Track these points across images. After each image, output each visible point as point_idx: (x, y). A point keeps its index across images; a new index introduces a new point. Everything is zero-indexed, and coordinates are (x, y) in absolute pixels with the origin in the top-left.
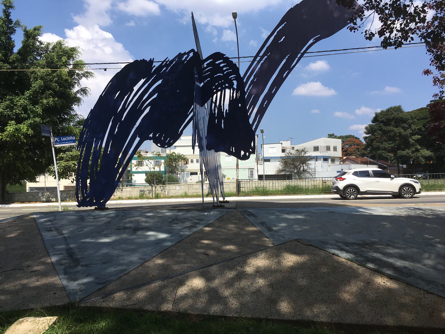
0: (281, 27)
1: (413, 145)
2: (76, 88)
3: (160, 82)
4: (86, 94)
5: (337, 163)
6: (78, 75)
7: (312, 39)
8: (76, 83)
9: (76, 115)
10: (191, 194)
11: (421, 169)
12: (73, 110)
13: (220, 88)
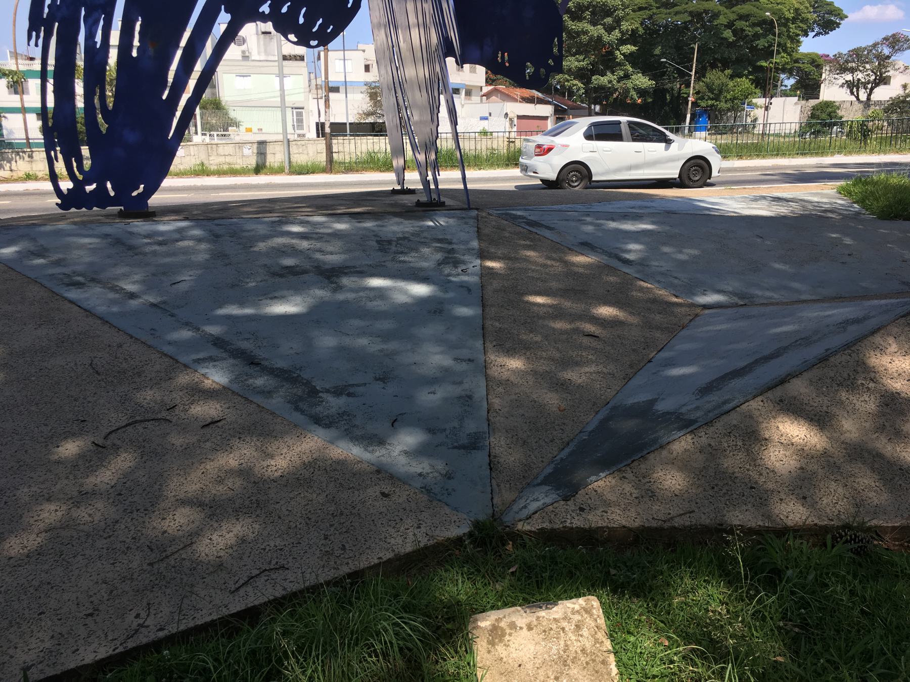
5: (475, 98)
10: (216, 168)
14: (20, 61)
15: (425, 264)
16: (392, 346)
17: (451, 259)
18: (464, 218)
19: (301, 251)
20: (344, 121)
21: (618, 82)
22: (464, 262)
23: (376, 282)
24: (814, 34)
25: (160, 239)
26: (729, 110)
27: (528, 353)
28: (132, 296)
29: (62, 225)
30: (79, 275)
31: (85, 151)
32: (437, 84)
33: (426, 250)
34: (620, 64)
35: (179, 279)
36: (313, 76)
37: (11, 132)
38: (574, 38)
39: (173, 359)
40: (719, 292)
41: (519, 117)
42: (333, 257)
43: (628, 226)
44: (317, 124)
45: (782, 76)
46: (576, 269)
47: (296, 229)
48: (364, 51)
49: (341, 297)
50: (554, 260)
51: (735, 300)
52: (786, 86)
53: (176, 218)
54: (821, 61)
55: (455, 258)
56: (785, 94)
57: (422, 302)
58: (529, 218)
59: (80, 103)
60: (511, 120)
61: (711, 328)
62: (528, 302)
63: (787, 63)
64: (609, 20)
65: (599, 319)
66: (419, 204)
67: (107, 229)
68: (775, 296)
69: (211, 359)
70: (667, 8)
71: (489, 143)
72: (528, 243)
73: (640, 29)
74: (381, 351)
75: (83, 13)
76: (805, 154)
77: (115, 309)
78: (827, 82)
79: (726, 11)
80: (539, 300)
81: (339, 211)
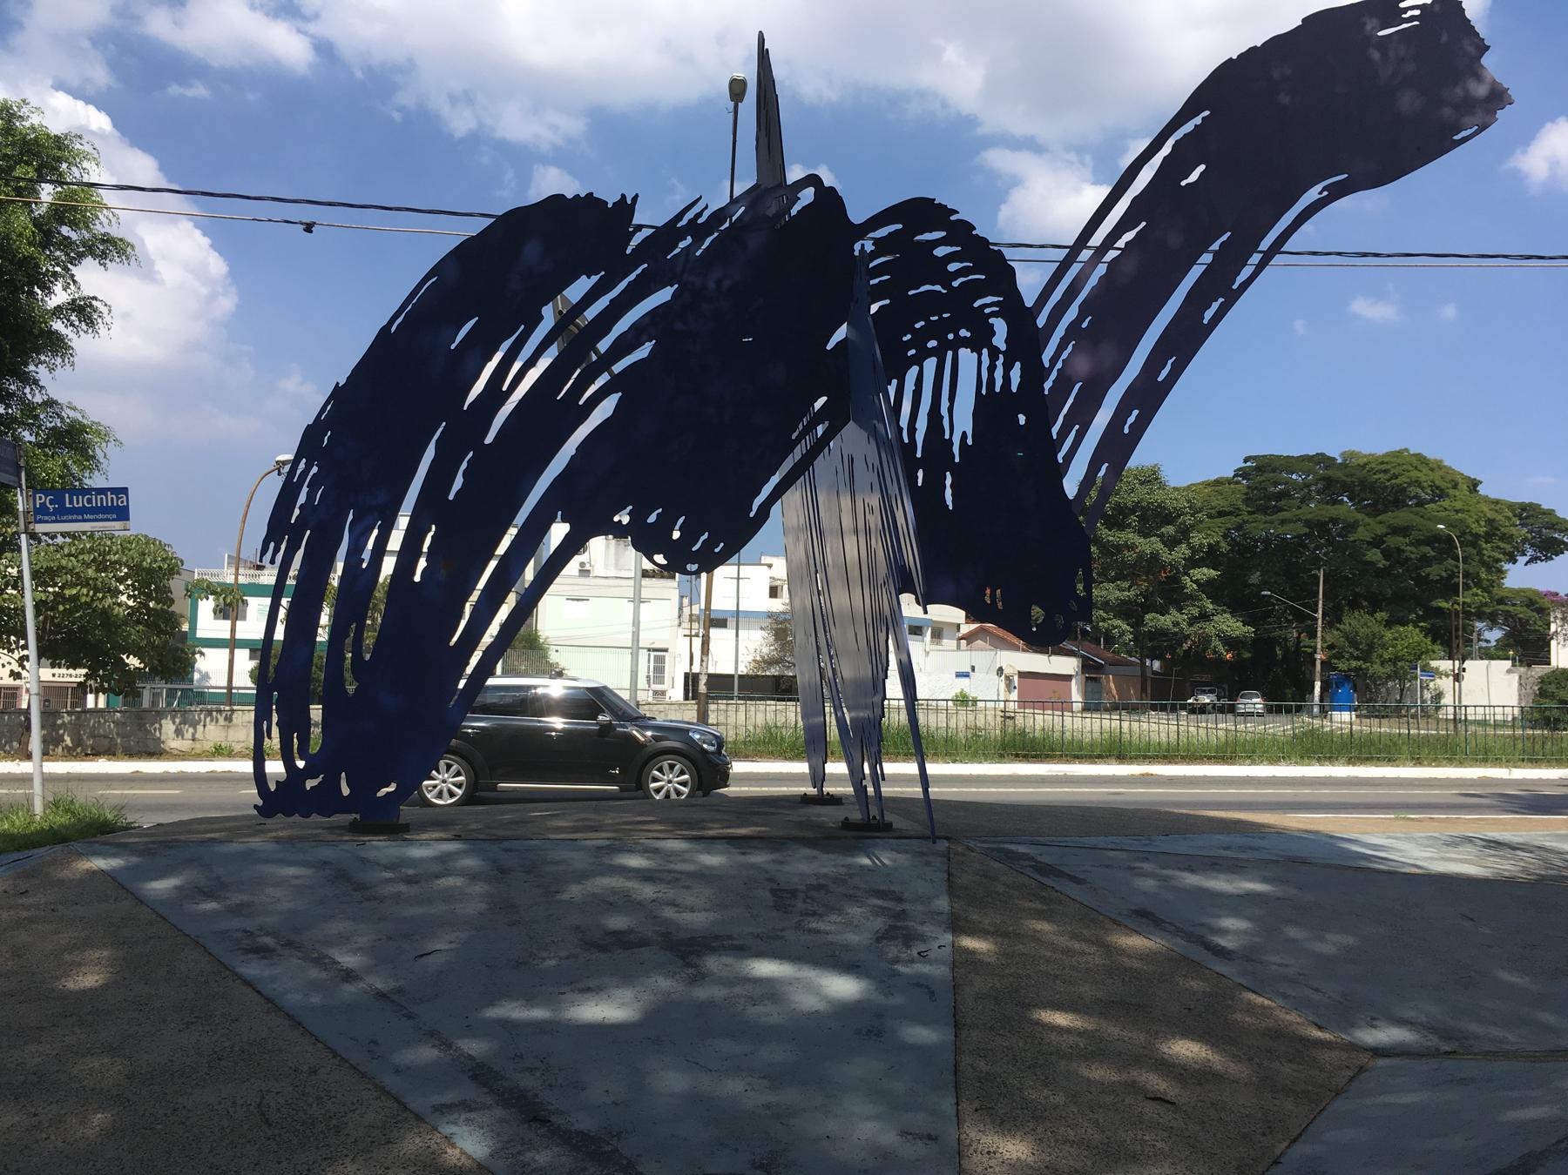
0: (1188, 127)
1: (1192, 597)
2: (59, 296)
3: (664, 295)
4: (91, 323)
6: (66, 243)
7: (1319, 187)
8: (55, 274)
9: (50, 403)
11: (1206, 678)
12: (36, 382)
13: (932, 344)
14: (241, 571)
15: (852, 938)
16: (789, 1096)
17: (900, 931)
18: (923, 854)
19: (639, 904)
20: (731, 671)
21: (1190, 625)
22: (922, 938)
23: (766, 968)
24: (1526, 559)
25: (410, 872)
26: (1389, 677)
27: (1040, 1130)
28: (349, 976)
29: (257, 843)
30: (267, 934)
31: (316, 712)
32: (889, 621)
33: (855, 911)
34: (1192, 597)
35: (431, 946)
36: (686, 601)
37: (206, 676)
38: (1113, 554)
39: (399, 1102)
40: (1401, 1022)
41: (1022, 675)
42: (696, 919)
43: (1220, 884)
44: (686, 676)
45: (1479, 625)
46: (1127, 962)
47: (635, 862)
48: (770, 566)
49: (702, 993)
50: (1085, 940)
51: (1434, 1041)
52: (1487, 641)
53: (442, 835)
54: (1545, 603)
55: (906, 928)
56: (1487, 655)
57: (845, 1011)
58: (1039, 859)
59: (323, 636)
60: (1007, 678)
61: (1390, 1099)
62: (1038, 1023)
63: (1486, 604)
64: (1170, 530)
65: (1173, 1065)
66: (847, 825)
67: (326, 853)
68: (1511, 1037)
69: (465, 1106)
70: (1266, 514)
71: (971, 717)
72: (1039, 906)
73: (1223, 544)
74: (767, 1106)
75: (351, 517)
76: (1537, 761)
77: (316, 999)
78: (1561, 638)
79: (1367, 520)
80: (1060, 1019)
81: (711, 833)
